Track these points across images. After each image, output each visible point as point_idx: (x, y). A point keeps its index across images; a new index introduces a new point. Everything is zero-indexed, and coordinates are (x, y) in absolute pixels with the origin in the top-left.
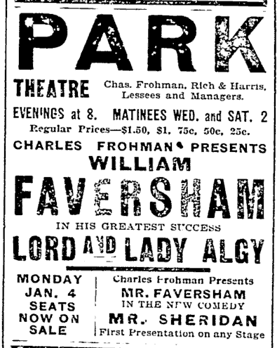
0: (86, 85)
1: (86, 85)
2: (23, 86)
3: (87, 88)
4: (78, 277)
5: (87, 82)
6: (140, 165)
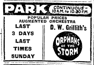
4: (29, 32)
6: (17, 27)
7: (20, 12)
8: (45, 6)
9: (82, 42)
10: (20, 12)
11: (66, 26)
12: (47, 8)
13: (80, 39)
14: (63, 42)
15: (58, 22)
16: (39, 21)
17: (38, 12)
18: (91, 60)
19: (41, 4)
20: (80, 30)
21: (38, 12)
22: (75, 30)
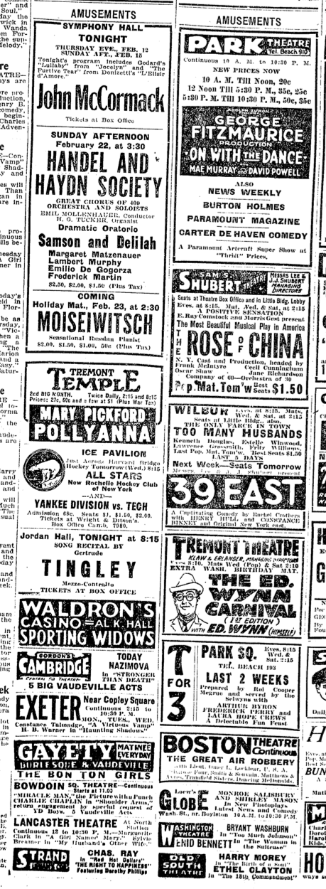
3: (205, 800)
5: (206, 793)
16: (120, 489)
18: (304, 526)
22: (131, 110)
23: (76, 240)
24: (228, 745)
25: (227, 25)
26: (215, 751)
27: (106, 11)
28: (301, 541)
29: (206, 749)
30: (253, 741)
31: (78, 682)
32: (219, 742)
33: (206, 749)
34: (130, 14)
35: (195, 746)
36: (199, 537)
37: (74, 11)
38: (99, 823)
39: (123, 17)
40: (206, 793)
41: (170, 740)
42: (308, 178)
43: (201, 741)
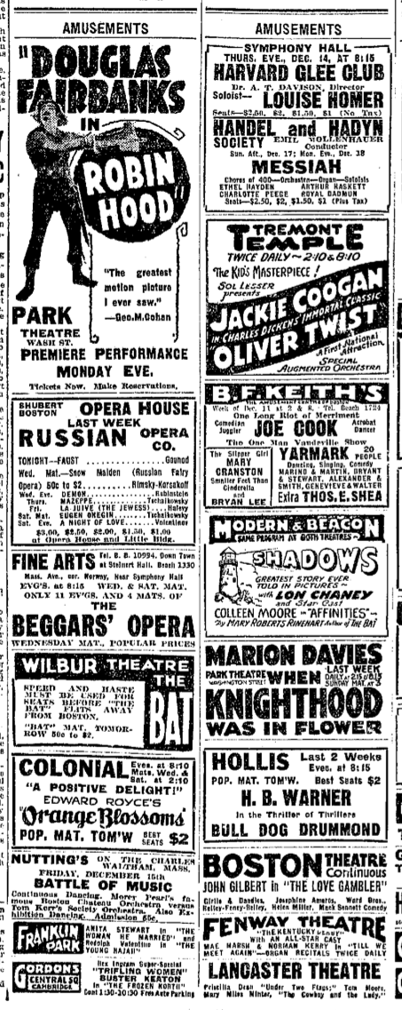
0: (382, 924)
1: (382, 924)
2: (317, 968)
3: (281, 428)
7: (398, 795)
8: (278, 388)
9: (121, 243)
10: (398, 795)
11: (293, 427)
12: (283, 392)
13: (208, 325)
14: (266, 319)
15: (30, 771)
16: (40, 412)
17: (279, 529)
19: (273, 386)
20: (232, 977)
21: (279, 529)
23: (374, 825)
24: (291, 865)
25: (269, 36)
26: (272, 874)
27: (107, 25)
28: (191, 402)
29: (260, 870)
30: (324, 860)
31: (28, 647)
32: (278, 862)
33: (260, 870)
34: (140, 27)
35: (245, 867)
36: (366, 837)
37: (259, 25)
38: (351, 970)
39: (324, 33)
40: (378, 964)
41: (211, 861)
42: (19, 81)
43: (254, 860)
